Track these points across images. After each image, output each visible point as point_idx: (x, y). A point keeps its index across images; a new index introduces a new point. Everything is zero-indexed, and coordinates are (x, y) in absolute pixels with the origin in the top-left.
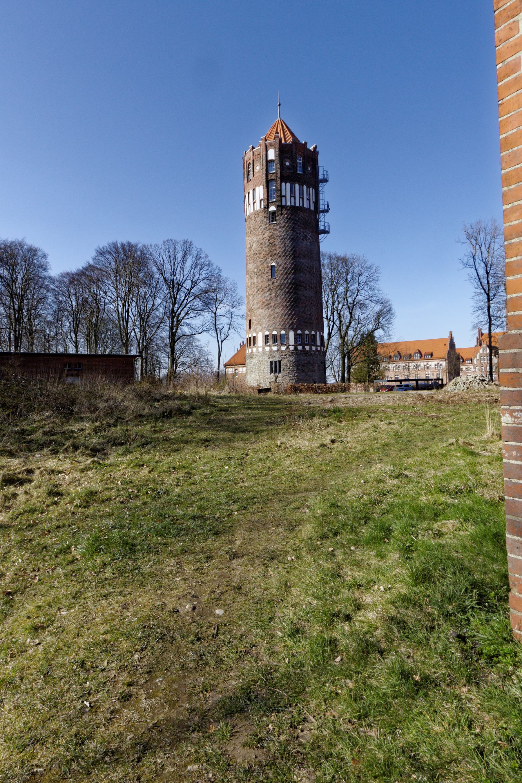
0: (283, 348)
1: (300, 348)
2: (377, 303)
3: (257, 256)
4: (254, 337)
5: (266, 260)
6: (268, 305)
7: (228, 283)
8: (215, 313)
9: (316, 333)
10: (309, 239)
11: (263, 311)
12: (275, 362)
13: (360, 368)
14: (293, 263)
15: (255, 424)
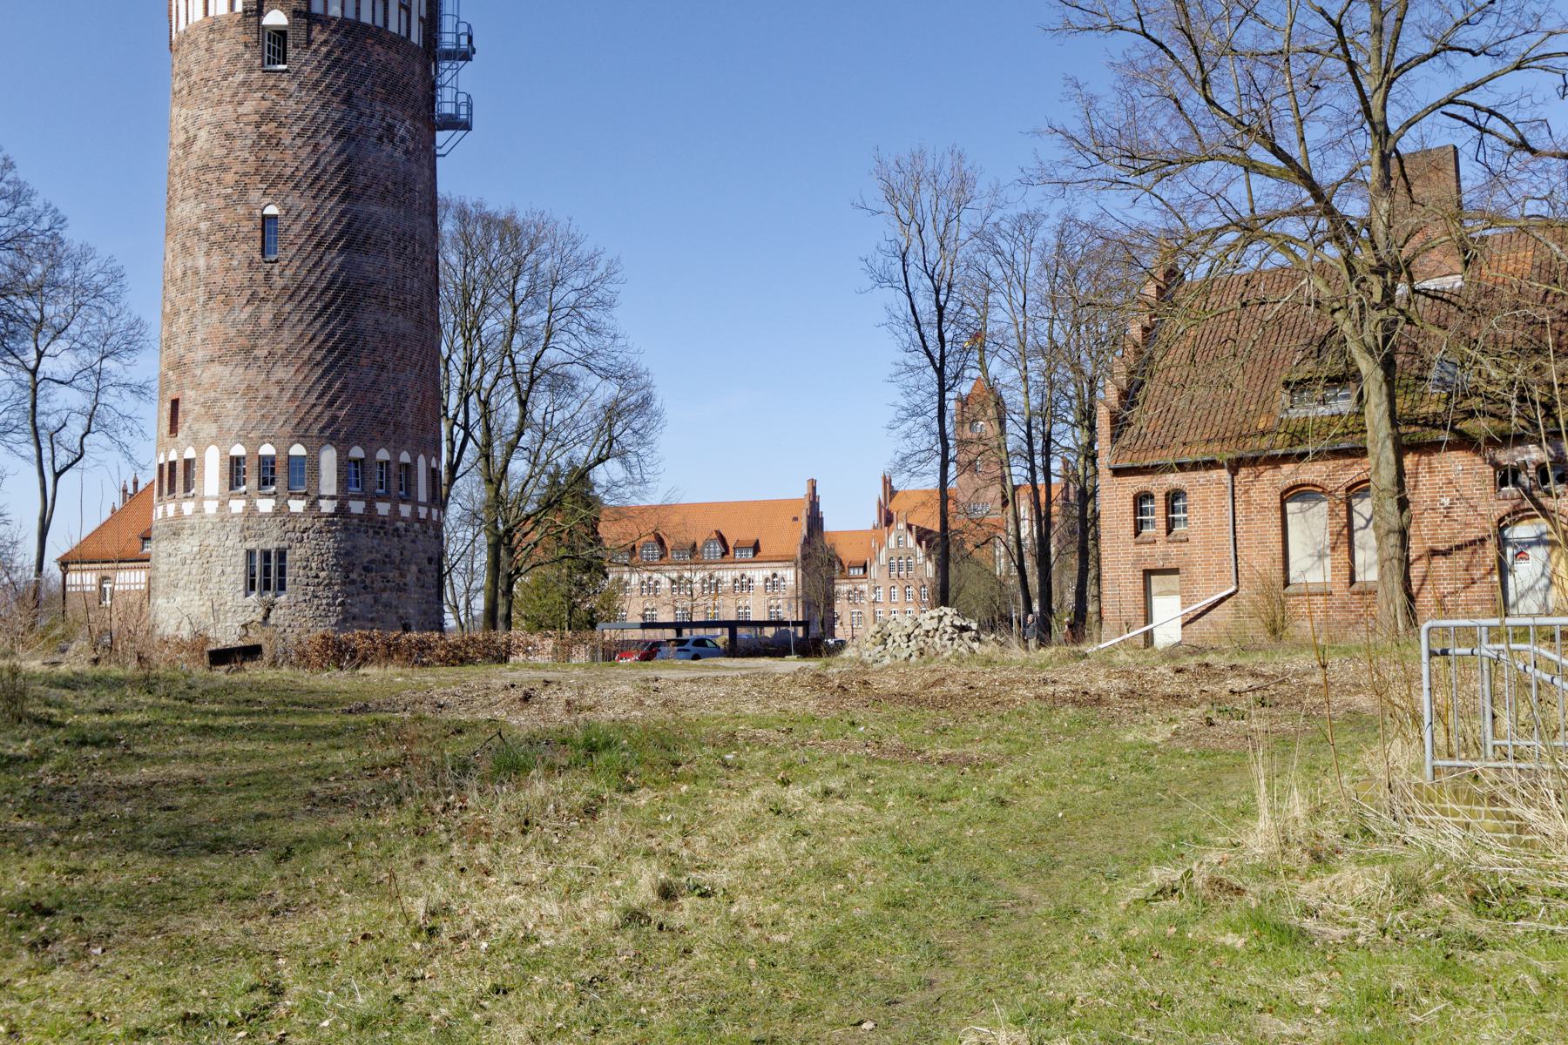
0: (297, 506)
1: (357, 507)
2: (606, 375)
3: (209, 177)
4: (188, 464)
5: (244, 191)
6: (248, 351)
7: (90, 267)
8: (34, 372)
9: (415, 460)
10: (403, 140)
11: (227, 371)
12: (266, 555)
13: (544, 585)
14: (343, 214)
15: (259, 807)
